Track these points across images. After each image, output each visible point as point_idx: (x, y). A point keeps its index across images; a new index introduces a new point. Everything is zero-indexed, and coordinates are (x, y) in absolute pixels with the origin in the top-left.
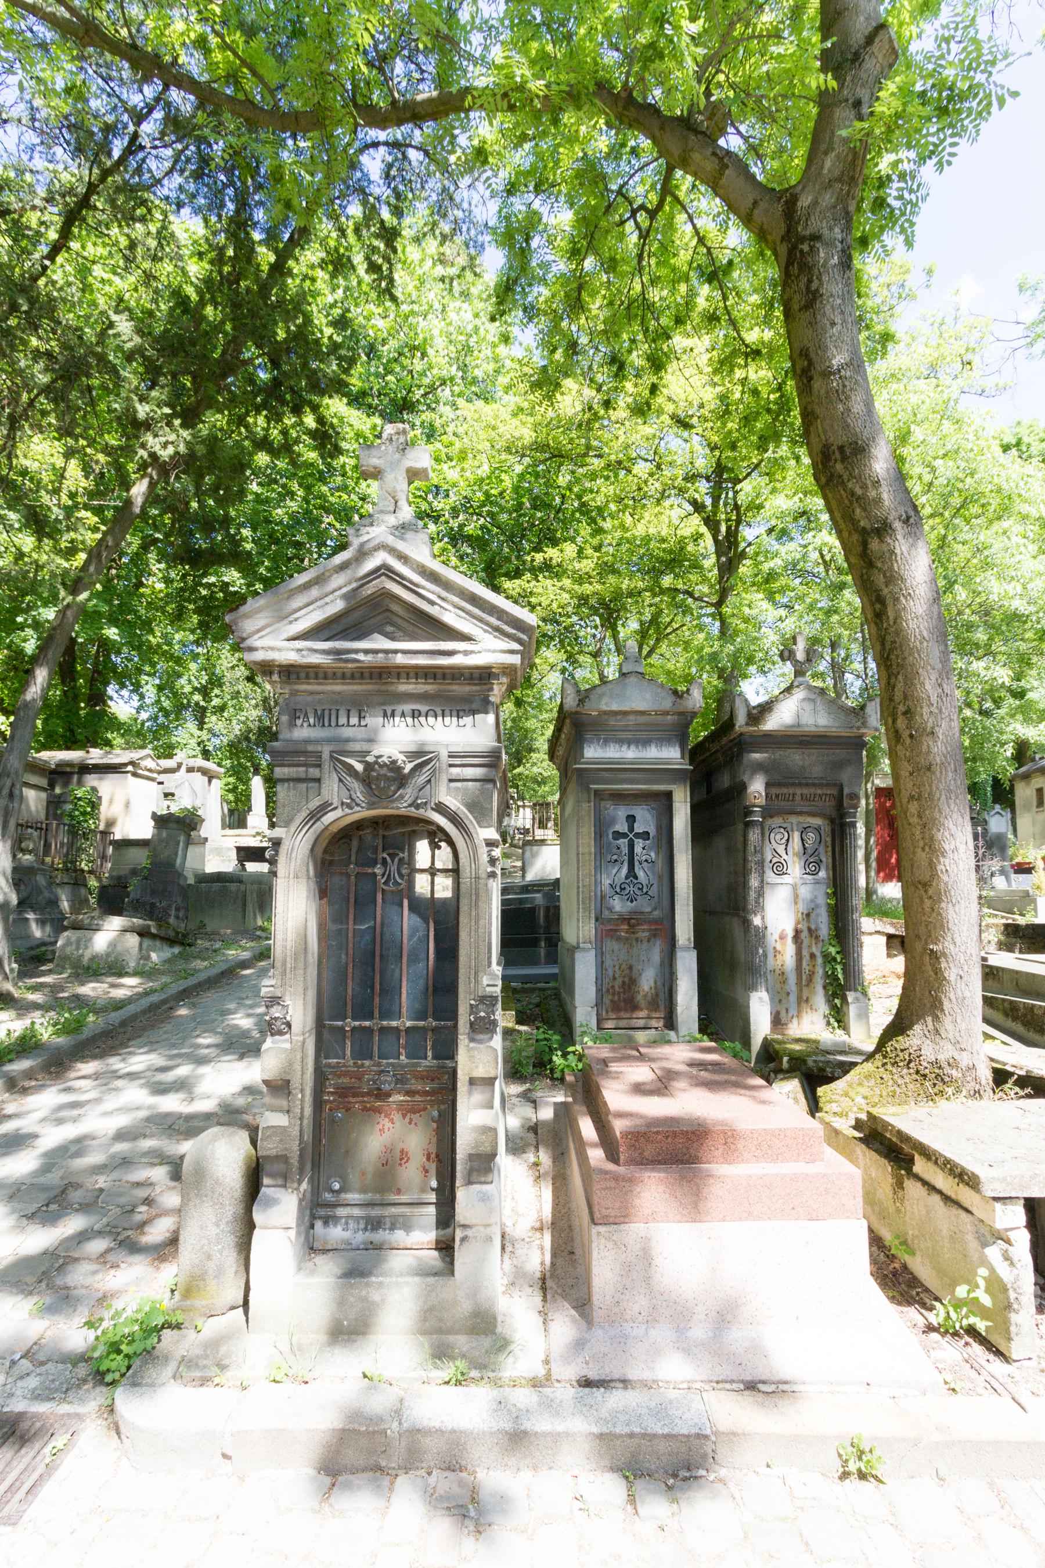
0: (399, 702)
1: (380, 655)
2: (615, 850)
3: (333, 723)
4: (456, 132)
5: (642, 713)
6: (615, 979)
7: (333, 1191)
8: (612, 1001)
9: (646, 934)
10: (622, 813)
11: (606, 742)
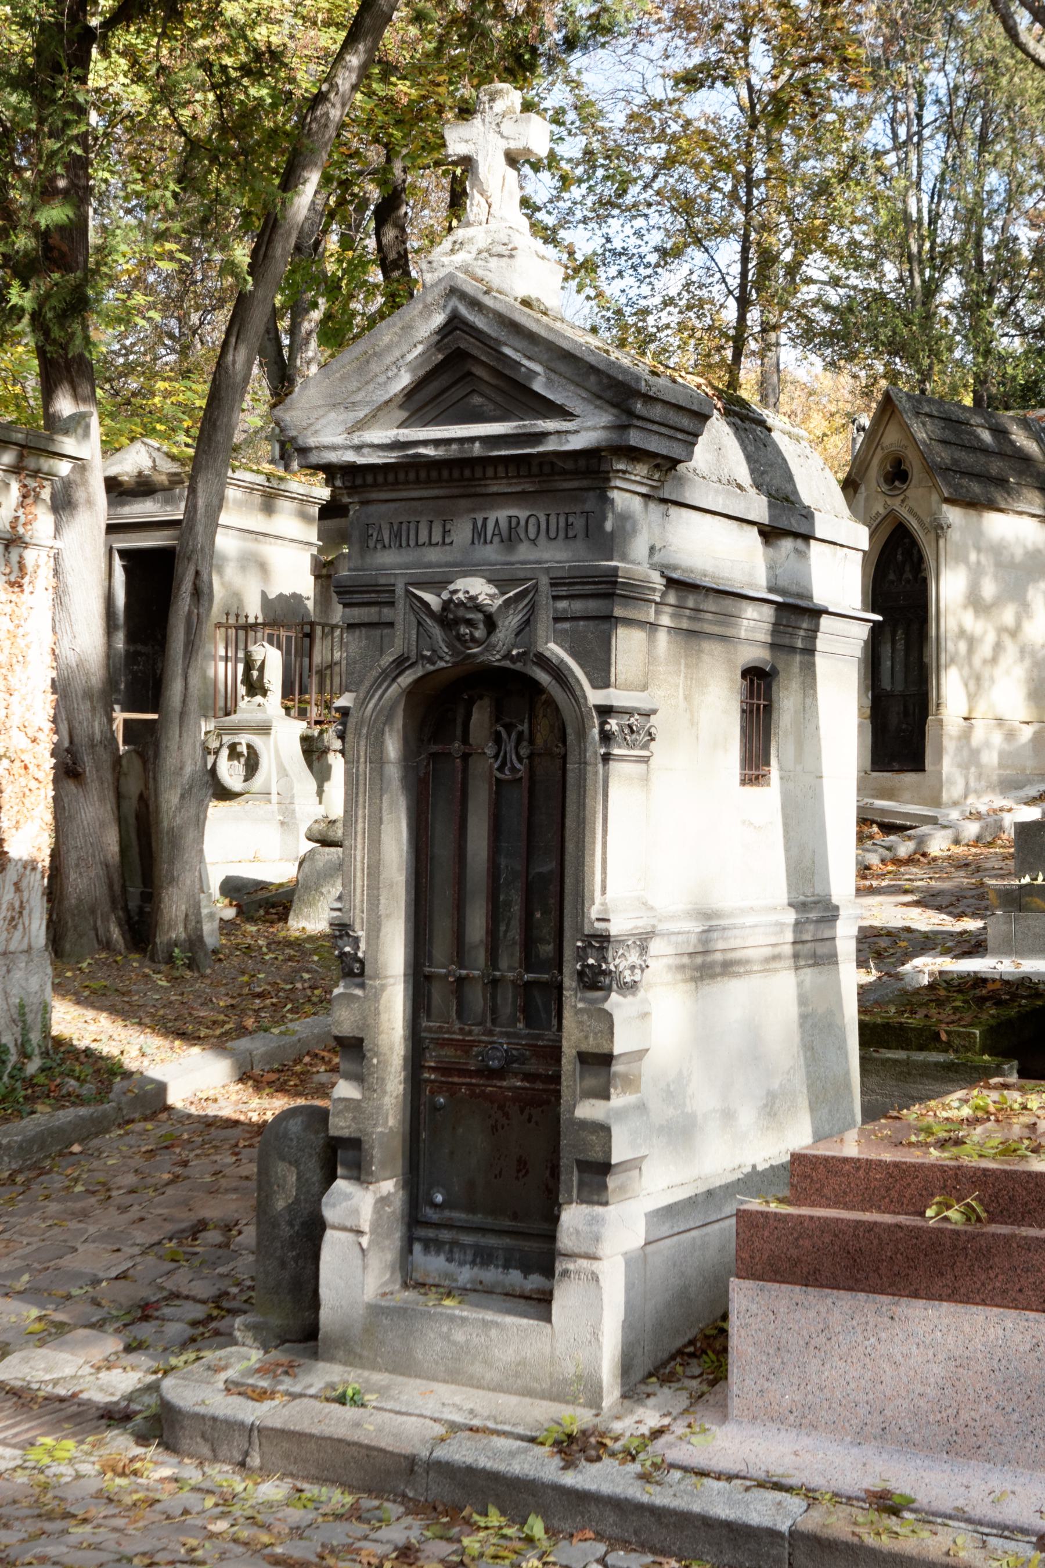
0: (492, 508)
1: (454, 447)
3: (412, 543)
4: (269, 101)
7: (435, 1206)
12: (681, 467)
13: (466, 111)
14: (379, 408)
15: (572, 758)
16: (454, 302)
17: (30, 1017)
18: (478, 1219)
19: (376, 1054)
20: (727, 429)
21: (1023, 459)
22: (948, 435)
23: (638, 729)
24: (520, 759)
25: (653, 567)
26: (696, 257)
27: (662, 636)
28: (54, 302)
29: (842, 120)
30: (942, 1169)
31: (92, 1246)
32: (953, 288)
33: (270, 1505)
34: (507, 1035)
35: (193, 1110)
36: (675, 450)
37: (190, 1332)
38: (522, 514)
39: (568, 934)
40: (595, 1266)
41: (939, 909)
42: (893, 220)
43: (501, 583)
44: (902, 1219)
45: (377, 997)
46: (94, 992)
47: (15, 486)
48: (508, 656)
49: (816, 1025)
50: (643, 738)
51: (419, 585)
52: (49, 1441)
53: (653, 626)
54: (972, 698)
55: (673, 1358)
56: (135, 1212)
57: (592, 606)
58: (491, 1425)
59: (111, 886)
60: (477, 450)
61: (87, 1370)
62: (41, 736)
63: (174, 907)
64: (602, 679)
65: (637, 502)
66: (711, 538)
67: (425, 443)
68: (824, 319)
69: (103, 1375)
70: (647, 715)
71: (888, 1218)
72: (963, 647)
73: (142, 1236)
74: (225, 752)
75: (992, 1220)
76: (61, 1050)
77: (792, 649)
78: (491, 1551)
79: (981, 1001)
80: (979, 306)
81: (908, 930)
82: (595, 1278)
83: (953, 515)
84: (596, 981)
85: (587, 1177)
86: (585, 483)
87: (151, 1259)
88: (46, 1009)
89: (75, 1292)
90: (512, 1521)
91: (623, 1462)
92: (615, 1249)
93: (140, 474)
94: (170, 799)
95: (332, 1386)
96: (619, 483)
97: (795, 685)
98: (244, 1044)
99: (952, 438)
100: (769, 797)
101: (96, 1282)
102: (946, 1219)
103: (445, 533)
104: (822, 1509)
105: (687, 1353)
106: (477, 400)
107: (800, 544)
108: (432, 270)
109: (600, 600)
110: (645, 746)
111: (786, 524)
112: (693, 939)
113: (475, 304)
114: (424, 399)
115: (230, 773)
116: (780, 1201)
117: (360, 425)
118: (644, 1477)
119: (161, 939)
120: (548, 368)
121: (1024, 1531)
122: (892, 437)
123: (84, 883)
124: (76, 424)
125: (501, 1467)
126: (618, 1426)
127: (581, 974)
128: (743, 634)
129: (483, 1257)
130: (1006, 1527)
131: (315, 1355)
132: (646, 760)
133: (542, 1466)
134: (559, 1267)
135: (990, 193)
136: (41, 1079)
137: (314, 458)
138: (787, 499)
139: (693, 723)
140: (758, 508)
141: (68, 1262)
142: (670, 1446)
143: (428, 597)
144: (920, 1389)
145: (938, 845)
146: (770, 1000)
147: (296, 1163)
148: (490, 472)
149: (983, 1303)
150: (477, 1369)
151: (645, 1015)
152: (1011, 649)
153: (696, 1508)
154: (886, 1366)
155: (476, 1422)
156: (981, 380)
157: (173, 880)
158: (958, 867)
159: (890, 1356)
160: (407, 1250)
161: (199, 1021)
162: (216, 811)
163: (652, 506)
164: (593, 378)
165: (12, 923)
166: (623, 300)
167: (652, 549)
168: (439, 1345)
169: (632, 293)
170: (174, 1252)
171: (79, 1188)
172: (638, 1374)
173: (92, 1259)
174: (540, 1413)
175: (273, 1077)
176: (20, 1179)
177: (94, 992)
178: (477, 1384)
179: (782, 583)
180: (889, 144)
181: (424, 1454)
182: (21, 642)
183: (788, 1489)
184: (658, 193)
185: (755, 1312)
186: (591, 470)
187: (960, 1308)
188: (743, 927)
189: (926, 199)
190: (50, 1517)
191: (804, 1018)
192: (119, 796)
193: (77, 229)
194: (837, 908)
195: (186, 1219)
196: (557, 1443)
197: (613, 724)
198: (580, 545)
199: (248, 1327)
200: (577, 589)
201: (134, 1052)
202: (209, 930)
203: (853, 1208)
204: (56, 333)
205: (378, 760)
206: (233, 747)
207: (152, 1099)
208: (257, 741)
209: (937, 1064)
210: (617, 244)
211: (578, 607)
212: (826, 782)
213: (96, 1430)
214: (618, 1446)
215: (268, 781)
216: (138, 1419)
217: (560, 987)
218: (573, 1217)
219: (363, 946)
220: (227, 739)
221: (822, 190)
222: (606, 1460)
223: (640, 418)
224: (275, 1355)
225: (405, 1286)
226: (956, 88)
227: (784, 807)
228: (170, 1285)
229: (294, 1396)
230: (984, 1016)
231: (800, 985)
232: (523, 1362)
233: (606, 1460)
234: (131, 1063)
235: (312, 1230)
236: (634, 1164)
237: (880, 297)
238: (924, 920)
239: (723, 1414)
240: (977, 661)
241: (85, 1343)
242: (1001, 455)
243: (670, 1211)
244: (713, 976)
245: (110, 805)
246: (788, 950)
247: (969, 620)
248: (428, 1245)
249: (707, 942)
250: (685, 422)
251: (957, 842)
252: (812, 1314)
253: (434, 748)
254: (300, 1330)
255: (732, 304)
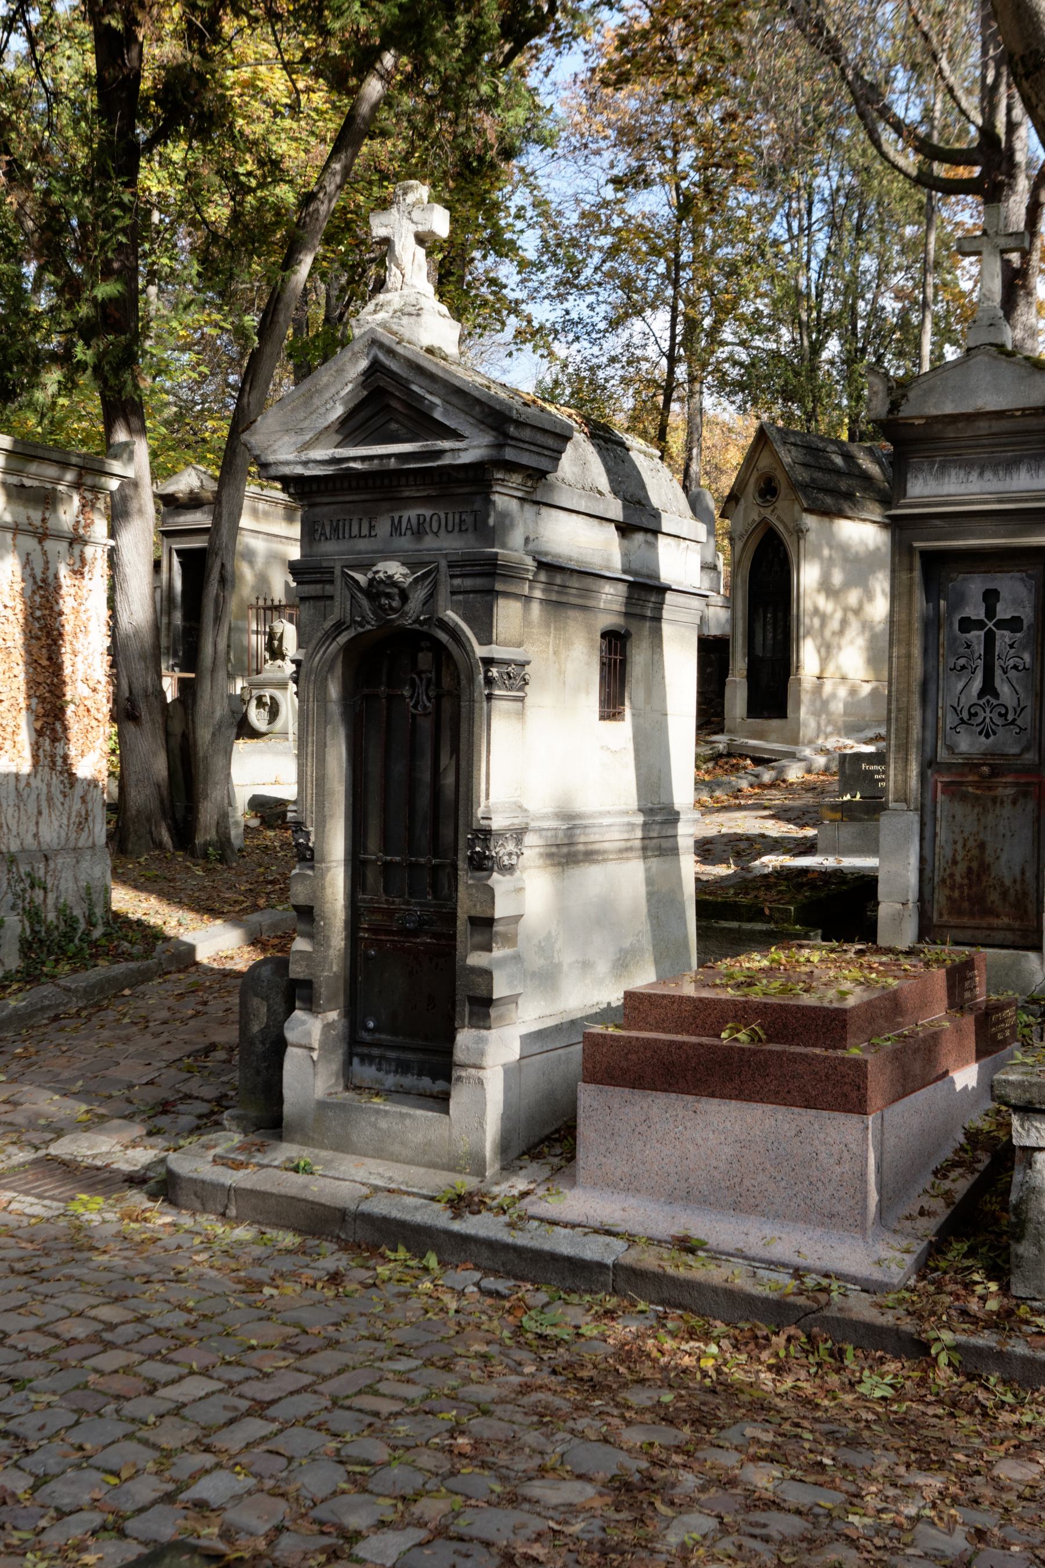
0: (406, 508)
2: (962, 650)
5: (1000, 414)
6: (955, 862)
7: (368, 1030)
8: (949, 898)
9: (1010, 791)
10: (975, 586)
11: (944, 468)
12: (549, 477)
13: (384, 204)
14: (321, 433)
15: (465, 697)
16: (375, 351)
17: (95, 897)
18: (399, 1039)
19: (323, 918)
20: (591, 448)
21: (865, 477)
22: (809, 459)
23: (516, 677)
24: (429, 699)
25: (527, 553)
26: (637, 325)
27: (536, 608)
28: (110, 358)
29: (749, 216)
30: (734, 1003)
31: (130, 1061)
32: (833, 347)
33: (240, 1243)
34: (420, 904)
35: (215, 965)
36: (543, 464)
37: (196, 1122)
38: (428, 513)
39: (461, 829)
40: (481, 1073)
41: (789, 821)
42: (786, 295)
43: (412, 565)
44: (704, 1040)
45: (323, 877)
46: (148, 879)
47: (76, 499)
48: (417, 621)
49: (660, 899)
50: (519, 682)
51: (352, 567)
52: (84, 1197)
53: (528, 599)
54: (824, 661)
55: (542, 1141)
56: (164, 1038)
57: (479, 582)
58: (403, 1188)
59: (162, 801)
60: (393, 463)
61: (118, 1148)
62: (100, 687)
63: (207, 814)
64: (486, 639)
65: (514, 504)
66: (577, 535)
67: (354, 459)
68: (734, 373)
69: (130, 1152)
70: (522, 665)
71: (694, 1039)
72: (816, 622)
73: (168, 1054)
74: (254, 703)
75: (770, 1040)
76: (119, 921)
77: (643, 617)
78: (398, 1276)
79: (802, 885)
80: (854, 362)
81: (763, 836)
82: (480, 1082)
83: (811, 521)
84: (482, 864)
85: (476, 1009)
86: (473, 489)
87: (173, 1071)
88: (107, 891)
89: (115, 1093)
90: (414, 1256)
91: (497, 1215)
92: (496, 1059)
93: (191, 492)
94: (204, 735)
95: (290, 1160)
96: (499, 489)
97: (645, 644)
98: (255, 917)
99: (812, 462)
100: (622, 731)
101: (131, 1086)
102: (736, 1040)
103: (371, 527)
104: (638, 1249)
105: (547, 1138)
106: (394, 426)
107: (650, 537)
108: (359, 327)
109: (485, 579)
110: (521, 689)
111: (638, 522)
112: (561, 834)
113: (390, 352)
114: (355, 426)
115: (257, 718)
116: (617, 1026)
117: (306, 446)
118: (511, 1225)
119: (199, 840)
120: (445, 401)
121: (785, 1265)
122: (764, 461)
123: (140, 798)
124: (125, 452)
125: (408, 1217)
126: (496, 1190)
127: (471, 859)
128: (602, 605)
129: (403, 1068)
130: (772, 1263)
131: (280, 1138)
132: (521, 699)
133: (439, 1217)
134: (456, 1073)
135: (864, 273)
136: (103, 942)
137: (273, 471)
138: (639, 503)
139: (561, 672)
140: (615, 509)
141: (113, 1072)
142: (532, 1203)
143: (358, 576)
144: (714, 1163)
145: (794, 773)
146: (623, 880)
147: (266, 998)
148: (403, 481)
149: (762, 1101)
150: (396, 1148)
151: (520, 890)
152: (854, 625)
153: (547, 1247)
154: (690, 1147)
155: (393, 1186)
156: (854, 420)
157: (206, 797)
158: (807, 790)
159: (693, 1140)
160: (348, 1063)
161: (225, 901)
162: (241, 746)
163: (527, 507)
164: (477, 409)
165: (80, 826)
166: (579, 358)
167: (527, 540)
168: (369, 1131)
169: (587, 353)
170: (190, 1066)
171: (126, 1020)
172: (514, 1153)
173: (130, 1070)
174: (440, 1180)
175: (276, 941)
176: (84, 1014)
177: (148, 879)
178: (396, 1159)
179: (634, 566)
180: (786, 237)
181: (353, 1207)
182: (84, 617)
183: (615, 1235)
184: (605, 274)
185: (598, 1109)
186: (477, 480)
187: (744, 1105)
188: (601, 826)
189: (814, 276)
190: (80, 1250)
191: (650, 895)
192: (168, 734)
193: (130, 299)
194: (678, 813)
195: (201, 1042)
196: (450, 1201)
197: (494, 672)
198: (470, 537)
199: (233, 1118)
200: (468, 570)
201: (174, 923)
202: (235, 834)
203: (669, 1032)
204: (112, 382)
205: (323, 699)
206: (259, 699)
207: (185, 956)
208: (278, 694)
209: (761, 932)
210: (574, 316)
211: (468, 583)
212: (670, 718)
213: (120, 1190)
214: (494, 1203)
215: (286, 724)
216: (152, 1182)
217: (455, 869)
218: (465, 1037)
219: (312, 838)
220: (255, 692)
221: (732, 271)
222: (484, 1213)
223: (513, 438)
224: (253, 1138)
225: (347, 1088)
226: (838, 189)
227: (635, 737)
228: (185, 1089)
229: (262, 1166)
230: (800, 897)
231: (647, 870)
232: (429, 1143)
233: (484, 1213)
234: (170, 931)
235: (279, 1046)
236: (513, 999)
237: (775, 355)
238: (775, 829)
239: (573, 1183)
240: (828, 633)
241: (119, 1130)
242: (849, 475)
243: (540, 1035)
244: (577, 862)
245: (160, 740)
246: (638, 844)
247: (823, 603)
248: (365, 1059)
249: (571, 836)
250: (550, 442)
251: (809, 771)
252: (637, 1109)
253: (366, 691)
254: (269, 1120)
255: (664, 362)
